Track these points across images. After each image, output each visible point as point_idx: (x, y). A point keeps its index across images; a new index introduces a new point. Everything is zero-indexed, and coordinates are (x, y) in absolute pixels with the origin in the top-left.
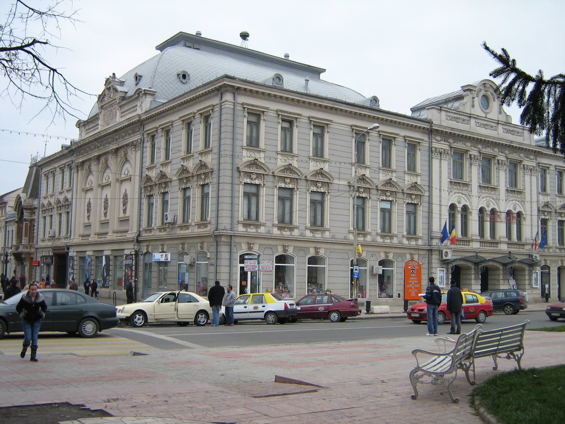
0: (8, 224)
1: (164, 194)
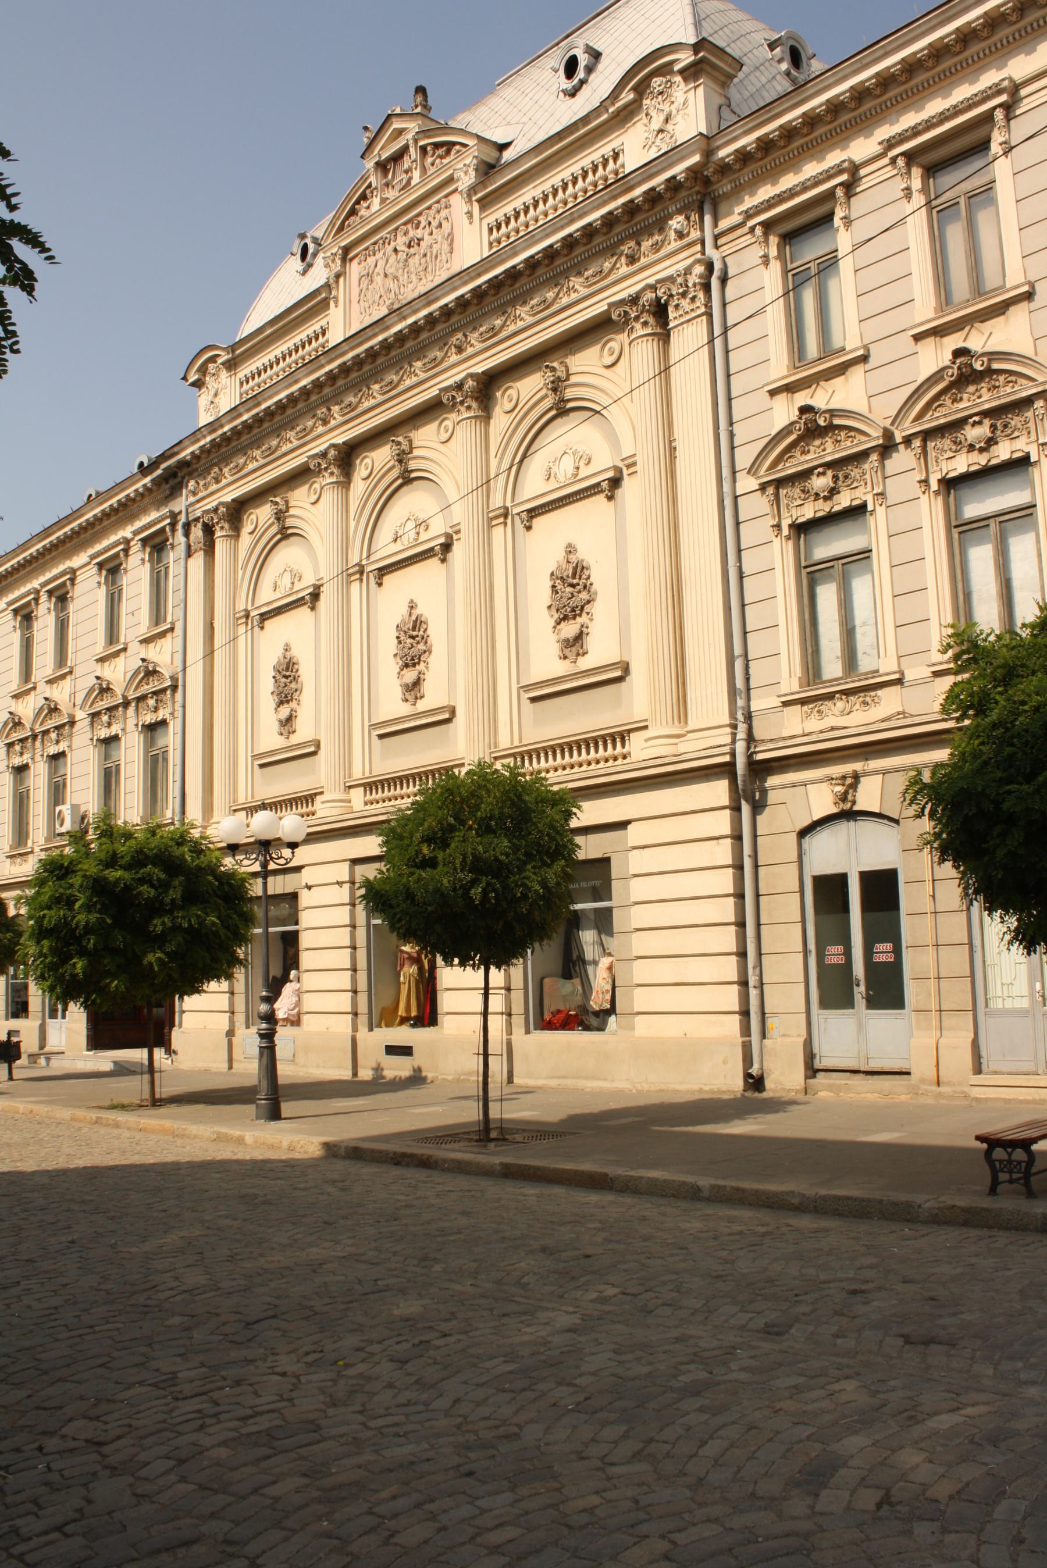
1: (153, 729)
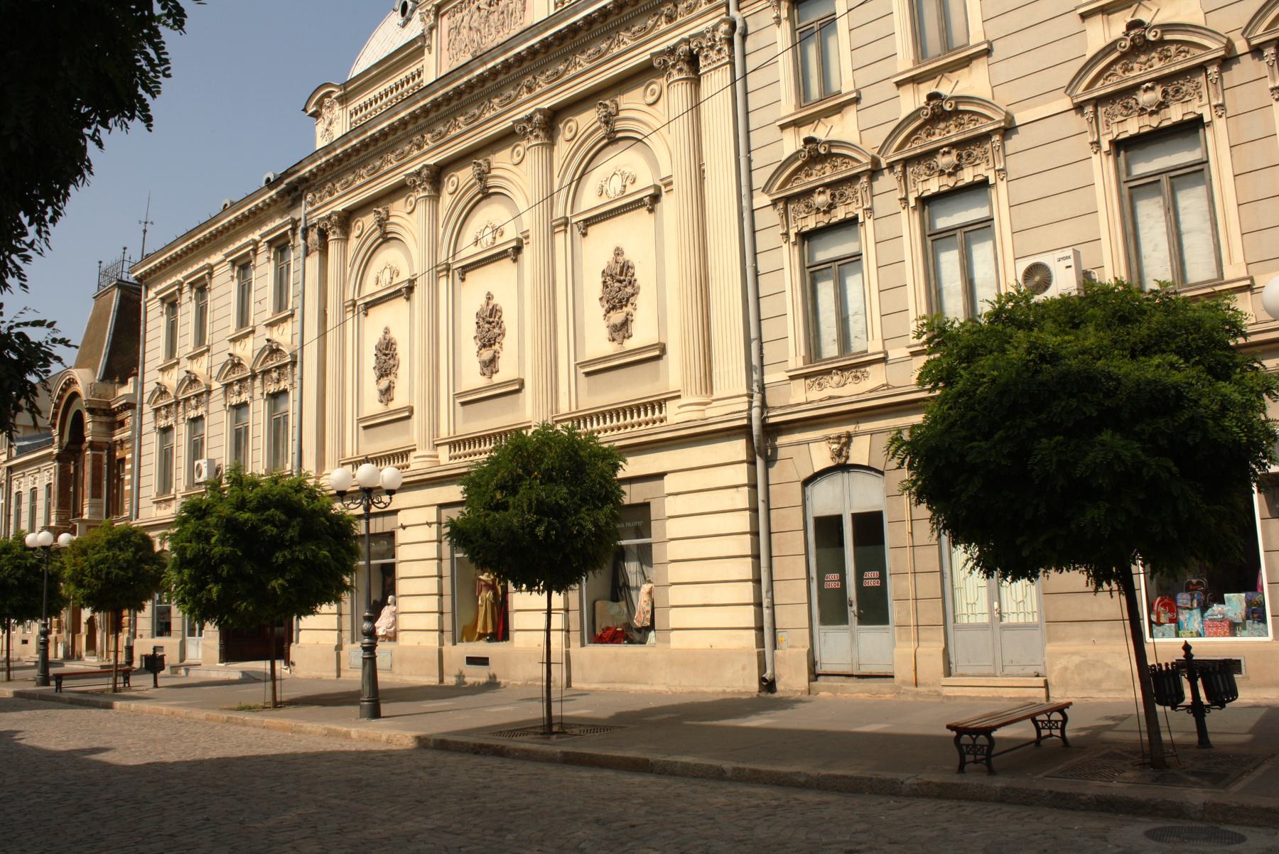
0: (16, 475)
